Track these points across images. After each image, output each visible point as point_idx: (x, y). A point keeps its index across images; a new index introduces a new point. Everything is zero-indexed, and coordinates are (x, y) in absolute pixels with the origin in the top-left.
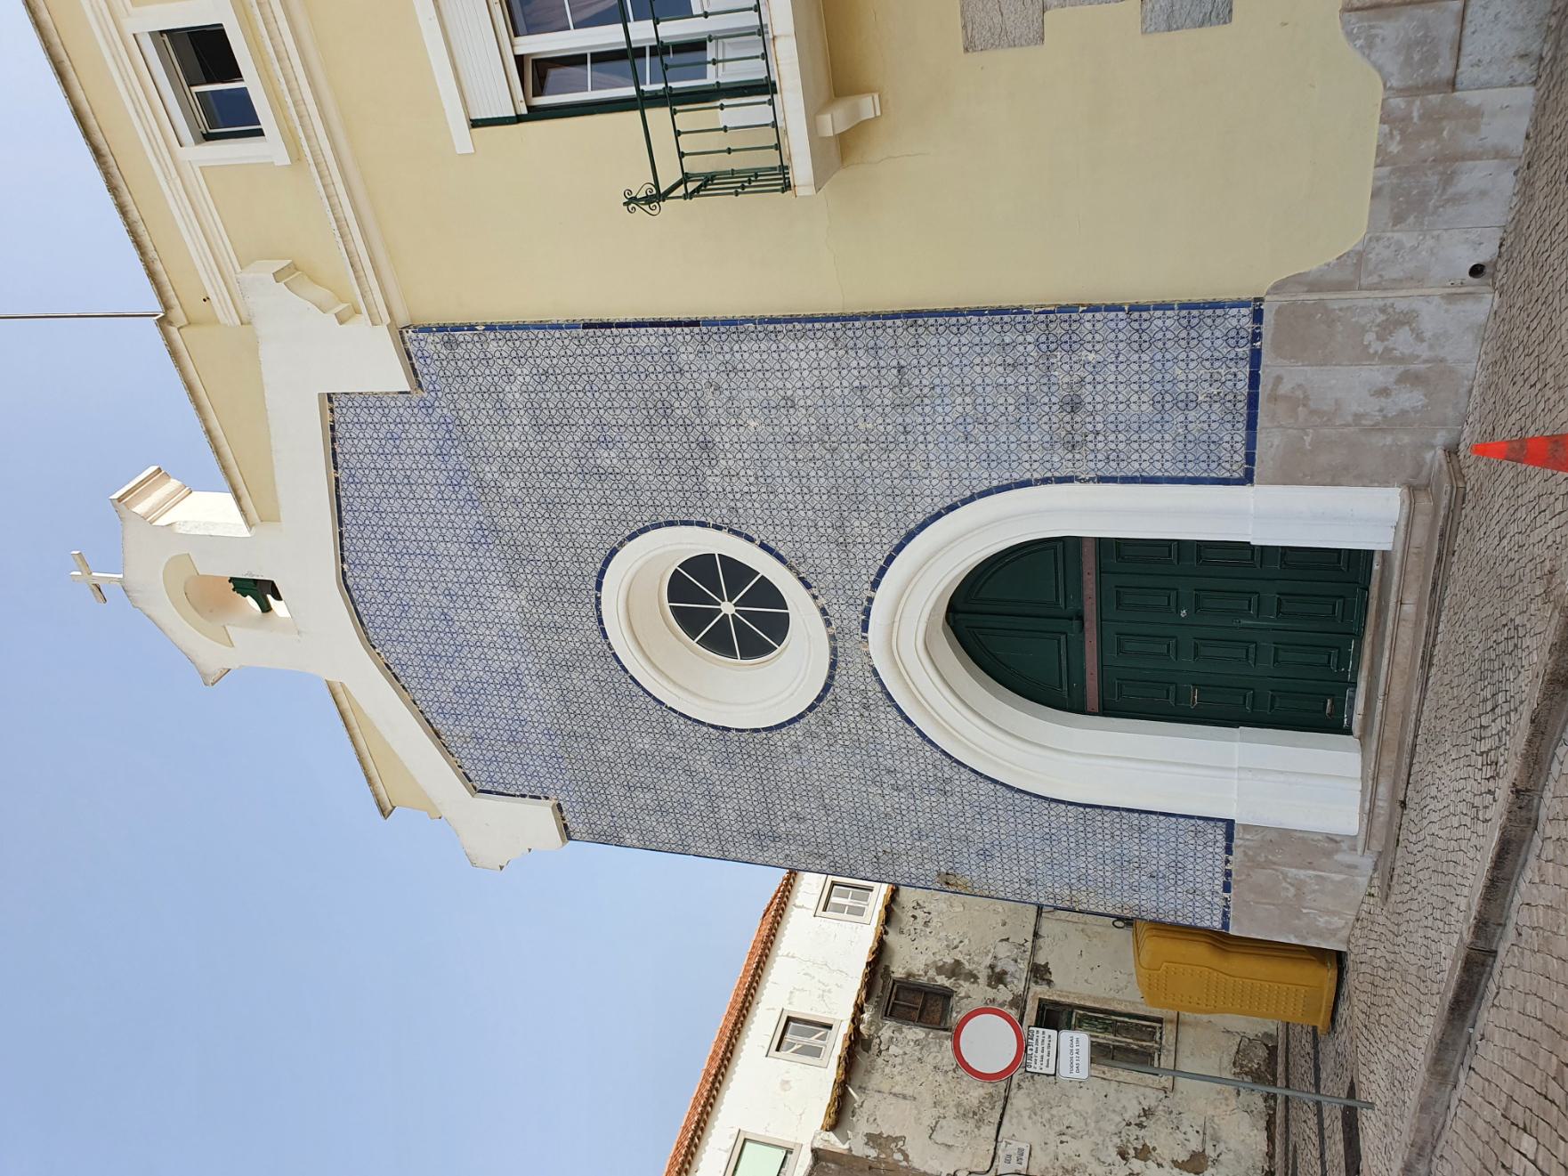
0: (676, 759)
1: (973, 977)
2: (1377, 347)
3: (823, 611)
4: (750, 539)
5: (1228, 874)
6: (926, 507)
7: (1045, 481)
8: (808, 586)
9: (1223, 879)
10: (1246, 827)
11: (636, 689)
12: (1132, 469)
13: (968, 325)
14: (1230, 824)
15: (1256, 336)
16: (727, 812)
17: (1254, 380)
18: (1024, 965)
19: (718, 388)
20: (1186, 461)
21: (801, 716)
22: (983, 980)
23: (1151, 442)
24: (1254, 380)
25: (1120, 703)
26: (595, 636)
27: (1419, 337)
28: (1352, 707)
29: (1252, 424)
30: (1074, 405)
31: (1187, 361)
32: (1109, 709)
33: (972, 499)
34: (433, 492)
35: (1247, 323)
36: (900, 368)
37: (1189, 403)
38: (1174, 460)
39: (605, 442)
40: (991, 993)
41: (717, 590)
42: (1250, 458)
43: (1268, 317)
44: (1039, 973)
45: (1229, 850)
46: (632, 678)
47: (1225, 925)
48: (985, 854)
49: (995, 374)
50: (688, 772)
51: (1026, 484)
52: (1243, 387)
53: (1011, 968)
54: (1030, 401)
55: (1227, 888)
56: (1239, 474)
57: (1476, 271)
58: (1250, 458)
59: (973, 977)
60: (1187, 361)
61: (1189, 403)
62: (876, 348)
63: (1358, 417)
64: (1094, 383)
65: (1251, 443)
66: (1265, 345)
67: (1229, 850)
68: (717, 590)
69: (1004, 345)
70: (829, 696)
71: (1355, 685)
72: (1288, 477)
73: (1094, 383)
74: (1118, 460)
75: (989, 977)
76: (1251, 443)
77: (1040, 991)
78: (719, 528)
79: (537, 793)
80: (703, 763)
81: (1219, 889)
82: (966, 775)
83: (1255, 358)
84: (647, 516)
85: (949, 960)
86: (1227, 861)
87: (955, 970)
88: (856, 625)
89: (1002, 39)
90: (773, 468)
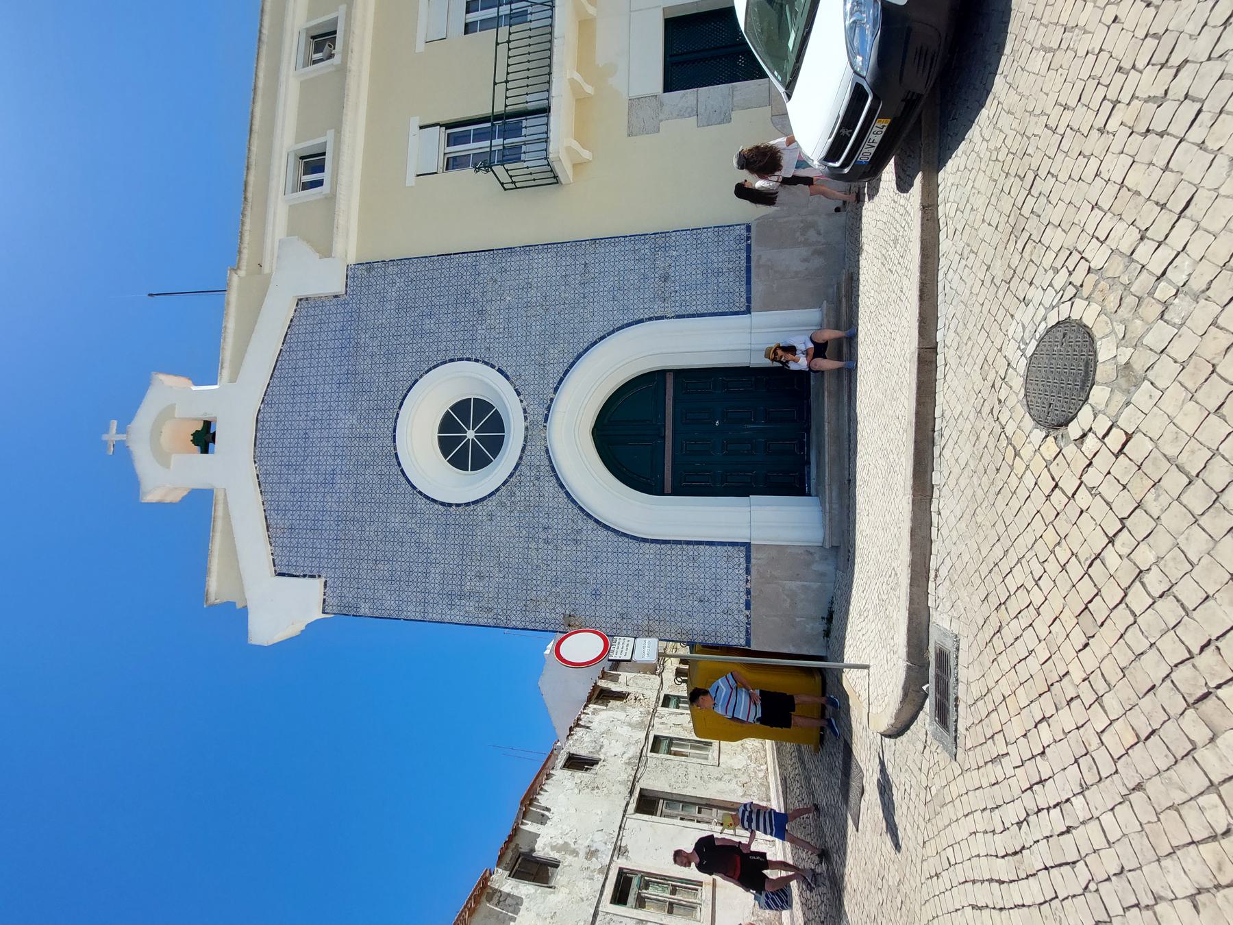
0: (411, 533)
1: (575, 853)
2: (802, 239)
3: (525, 411)
4: (493, 366)
5: (748, 592)
6: (590, 338)
7: (650, 319)
8: (519, 394)
9: (744, 597)
10: (761, 547)
11: (402, 479)
12: (692, 310)
13: (619, 242)
14: (747, 546)
15: (748, 238)
16: (435, 576)
17: (749, 259)
18: (611, 847)
19: (495, 281)
20: (718, 304)
21: (497, 490)
22: (582, 854)
23: (701, 295)
24: (749, 259)
25: (684, 487)
26: (389, 442)
27: (819, 233)
28: (809, 479)
29: (748, 282)
30: (666, 278)
31: (718, 252)
32: (676, 492)
33: (613, 332)
34: (330, 353)
35: (744, 232)
36: (586, 264)
37: (719, 273)
38: (713, 304)
39: (430, 316)
40: (586, 864)
41: (467, 443)
42: (749, 300)
43: (753, 229)
44: (619, 850)
45: (748, 571)
46: (402, 471)
47: (748, 642)
48: (596, 594)
49: (630, 264)
50: (418, 543)
51: (641, 321)
52: (744, 263)
53: (602, 847)
54: (645, 277)
55: (748, 606)
56: (744, 308)
57: (837, 210)
58: (749, 300)
59: (575, 853)
60: (718, 252)
61: (719, 273)
62: (575, 255)
63: (797, 273)
64: (675, 266)
65: (749, 291)
66: (753, 242)
67: (748, 571)
68: (467, 443)
69: (635, 250)
70: (517, 473)
71: (809, 463)
72: (767, 307)
73: (675, 266)
74: (686, 306)
75: (587, 854)
76: (749, 291)
77: (621, 862)
78: (477, 361)
79: (314, 573)
80: (427, 535)
81: (742, 606)
82: (591, 524)
83: (749, 247)
84: (440, 357)
85: (561, 842)
86: (747, 581)
87: (565, 848)
88: (541, 418)
89: (644, 131)
90: (514, 323)
